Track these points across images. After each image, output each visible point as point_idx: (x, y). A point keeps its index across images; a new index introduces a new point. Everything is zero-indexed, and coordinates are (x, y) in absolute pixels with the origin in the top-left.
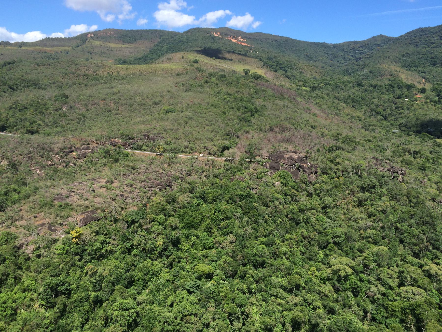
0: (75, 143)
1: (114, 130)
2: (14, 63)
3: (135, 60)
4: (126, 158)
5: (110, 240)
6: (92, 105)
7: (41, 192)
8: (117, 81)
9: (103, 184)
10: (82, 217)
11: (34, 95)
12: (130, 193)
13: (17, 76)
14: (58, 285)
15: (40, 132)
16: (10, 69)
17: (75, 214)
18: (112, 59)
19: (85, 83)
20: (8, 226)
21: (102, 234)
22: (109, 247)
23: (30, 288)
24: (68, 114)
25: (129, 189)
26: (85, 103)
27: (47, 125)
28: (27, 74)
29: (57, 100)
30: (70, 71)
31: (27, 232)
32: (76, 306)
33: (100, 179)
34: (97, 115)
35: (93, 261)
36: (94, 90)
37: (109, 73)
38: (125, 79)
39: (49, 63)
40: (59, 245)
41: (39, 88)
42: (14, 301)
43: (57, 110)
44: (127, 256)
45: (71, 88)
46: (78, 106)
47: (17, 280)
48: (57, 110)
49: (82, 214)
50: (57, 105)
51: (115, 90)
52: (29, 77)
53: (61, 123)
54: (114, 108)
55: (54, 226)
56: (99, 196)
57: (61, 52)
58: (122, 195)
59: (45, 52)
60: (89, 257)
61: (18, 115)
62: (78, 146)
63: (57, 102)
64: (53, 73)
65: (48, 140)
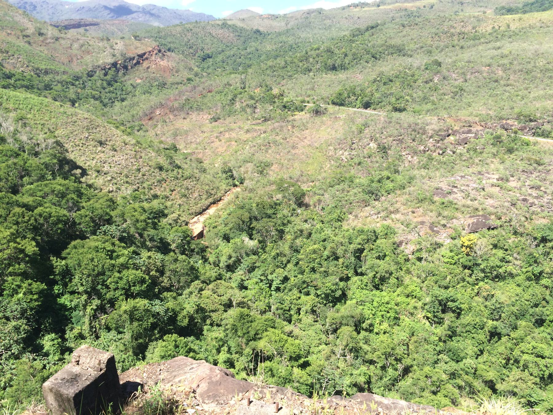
0: (453, 125)
1: (505, 108)
2: (377, 26)
3: (524, 6)
4: (525, 147)
5: (511, 258)
6: (472, 73)
7: (417, 182)
8: (506, 38)
9: (495, 181)
10: (470, 221)
11: (401, 64)
12: (537, 198)
13: (380, 42)
14: (448, 300)
15: (408, 110)
16: (373, 35)
17: (461, 216)
18: (491, 9)
19: (461, 45)
20: (384, 219)
21: (502, 248)
22: (510, 268)
23: (414, 294)
24: (440, 87)
25: (534, 193)
26: (463, 71)
27: (416, 101)
28: (391, 38)
29: (427, 69)
30: (441, 30)
31: (405, 228)
32: (469, 331)
33: (488, 173)
34: (479, 87)
35: (486, 281)
36: (474, 53)
37: (494, 27)
38: (518, 35)
39: (416, 22)
40: (444, 251)
41: (404, 56)
42: (397, 305)
43: (426, 82)
44: (534, 284)
45: (443, 53)
46: (454, 75)
47: (400, 282)
48: (426, 82)
49: (471, 217)
50: (427, 75)
51: (506, 52)
52: (392, 42)
53: (431, 98)
54: (502, 77)
55: (436, 227)
56: (491, 196)
57: (424, 7)
58: (525, 200)
59: (406, 10)
60: (483, 275)
61: (383, 89)
62: (456, 128)
63: (428, 72)
64: (421, 34)
65: (420, 120)
